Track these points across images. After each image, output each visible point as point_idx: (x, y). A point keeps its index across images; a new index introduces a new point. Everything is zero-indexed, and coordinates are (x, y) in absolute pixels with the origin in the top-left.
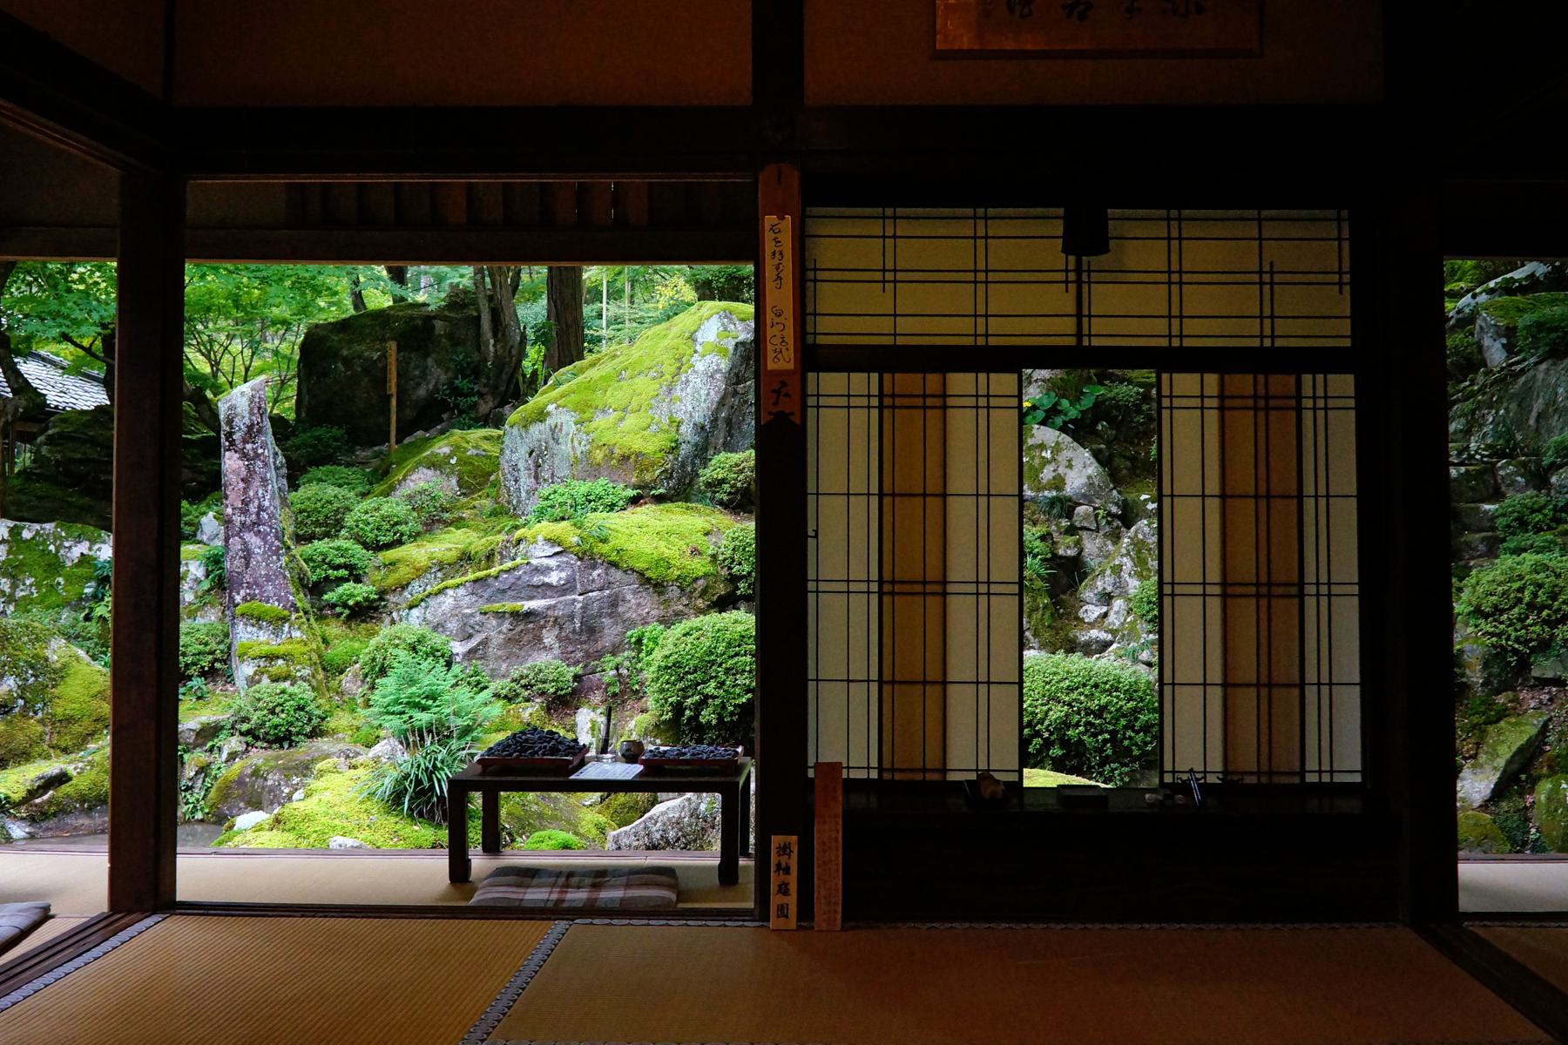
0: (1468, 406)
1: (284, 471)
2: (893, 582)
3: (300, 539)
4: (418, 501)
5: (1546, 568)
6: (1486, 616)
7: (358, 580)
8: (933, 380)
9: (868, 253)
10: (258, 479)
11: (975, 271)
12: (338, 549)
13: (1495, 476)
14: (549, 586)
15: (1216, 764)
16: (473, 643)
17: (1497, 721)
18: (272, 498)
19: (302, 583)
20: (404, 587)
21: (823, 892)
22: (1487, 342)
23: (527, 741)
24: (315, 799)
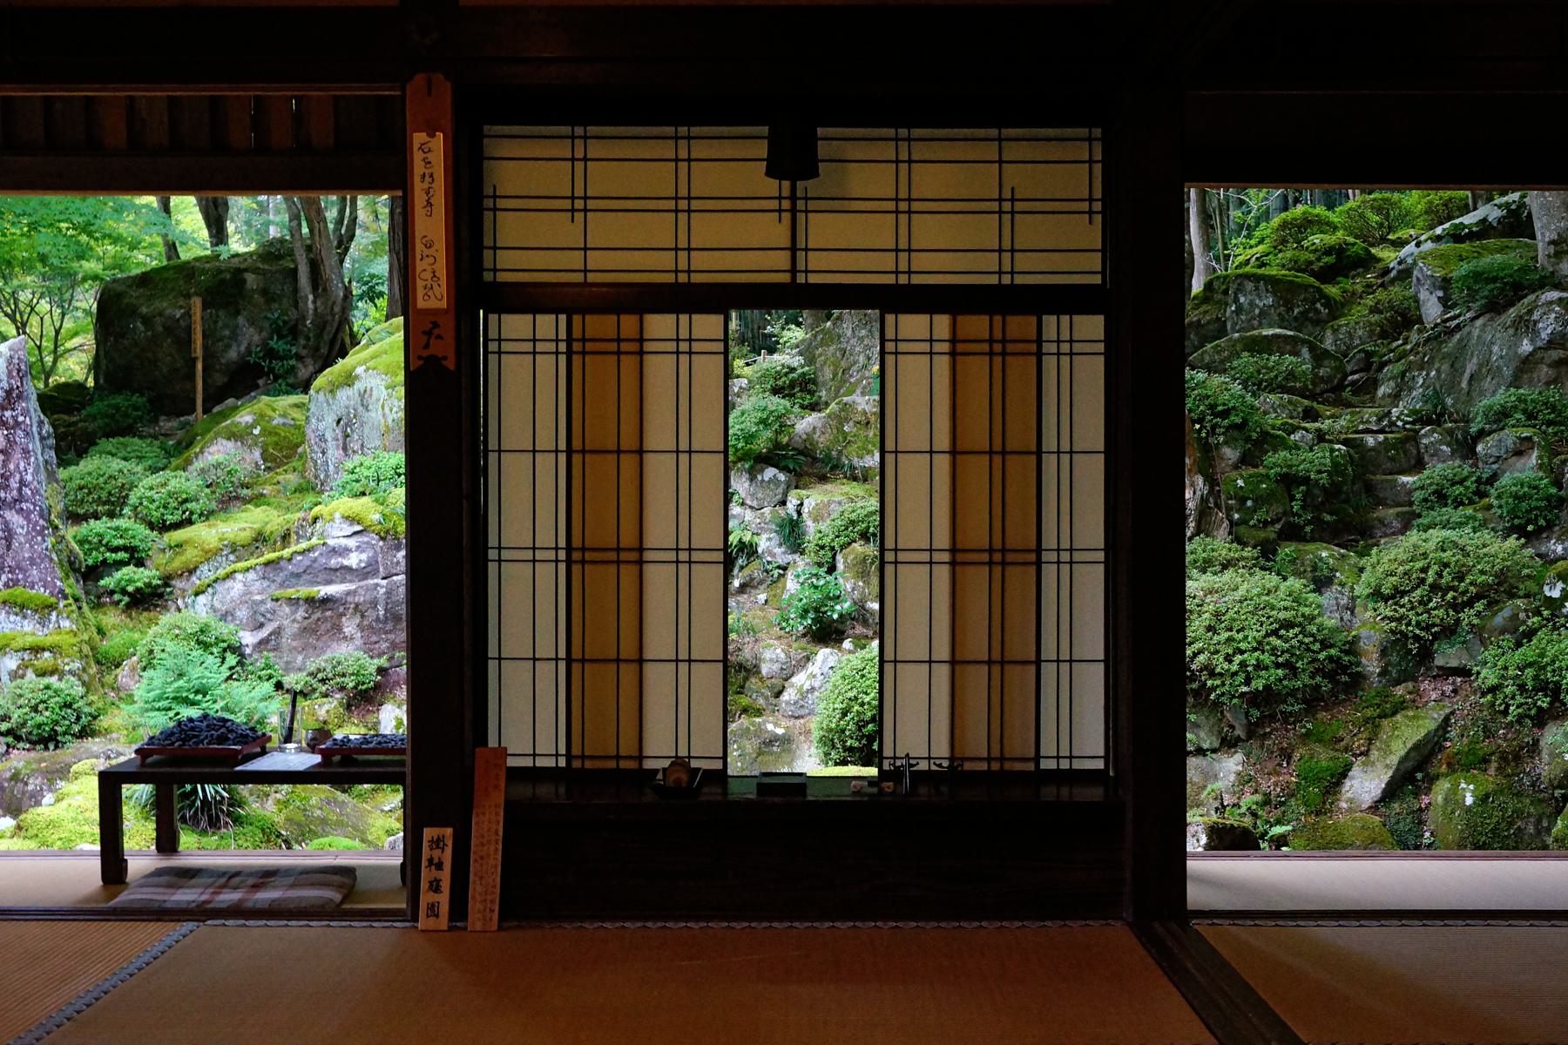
0: (1398, 368)
1: (52, 441)
2: (583, 549)
3: (75, 518)
4: (211, 478)
5: (1455, 545)
6: (1386, 599)
7: (140, 563)
8: (629, 322)
9: (553, 177)
10: (18, 449)
11: (676, 198)
12: (117, 529)
13: (1417, 444)
14: (349, 569)
15: (942, 749)
16: (264, 633)
17: (1394, 714)
18: (36, 471)
19: (72, 566)
20: (191, 572)
21: (479, 889)
22: (1423, 295)
23: (193, 729)
24: (64, 804)
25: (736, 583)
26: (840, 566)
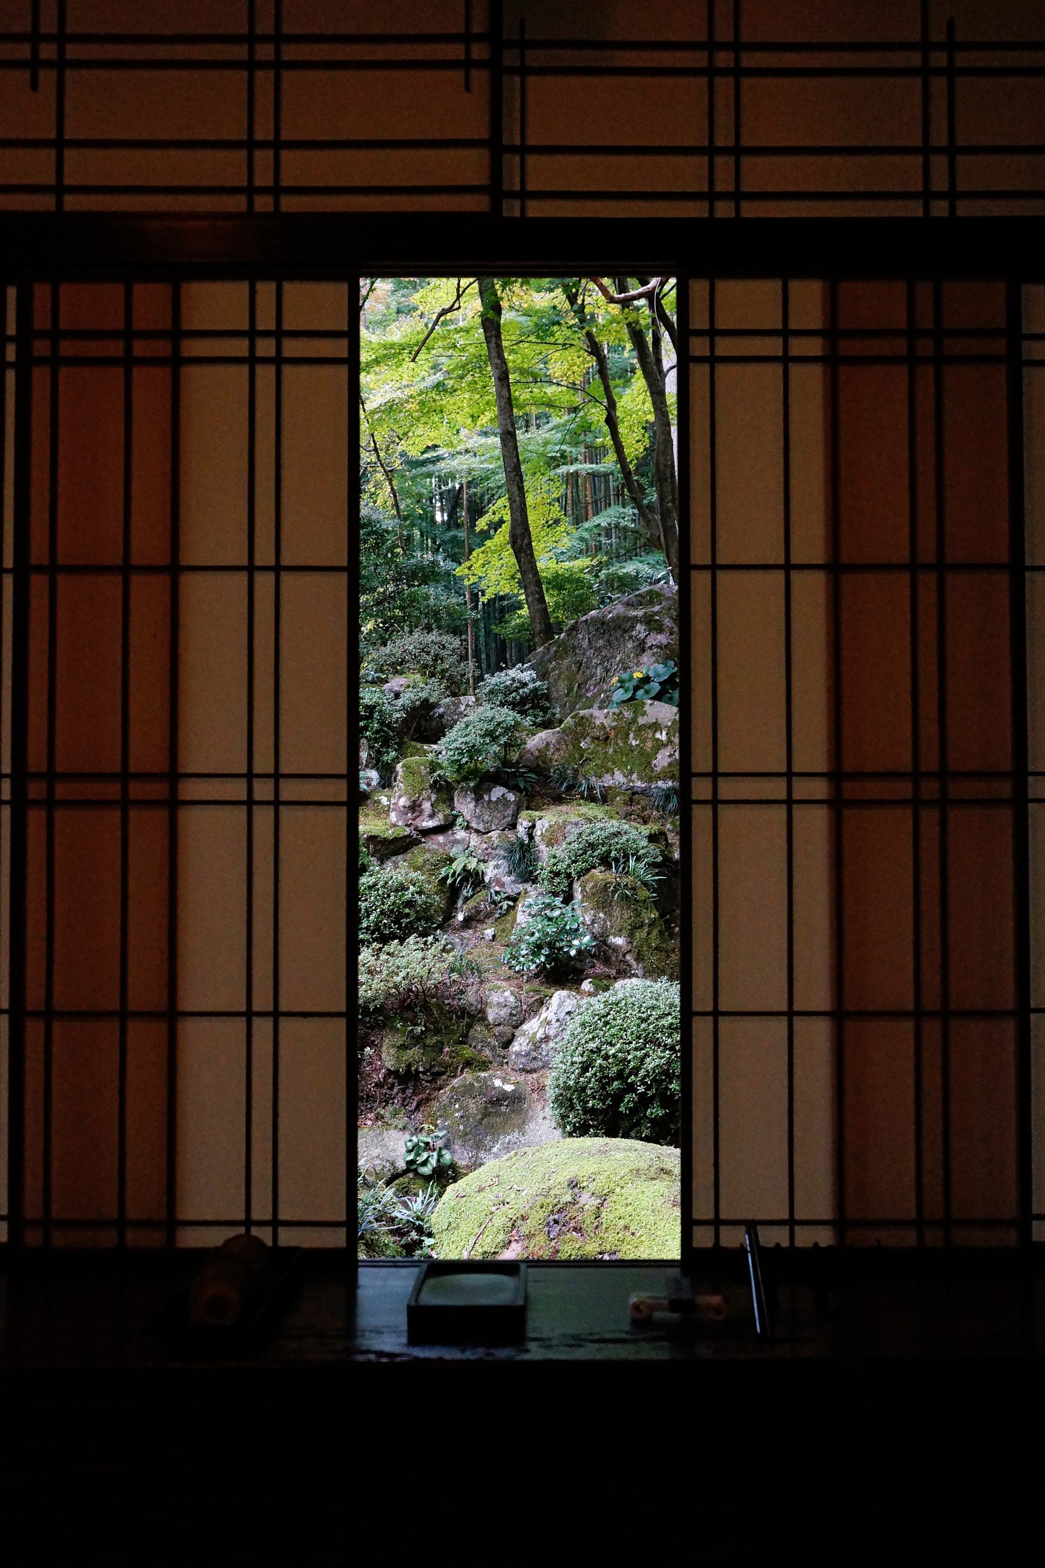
8: (150, 301)
15: (817, 1199)
25: (460, 917)
26: (578, 896)
